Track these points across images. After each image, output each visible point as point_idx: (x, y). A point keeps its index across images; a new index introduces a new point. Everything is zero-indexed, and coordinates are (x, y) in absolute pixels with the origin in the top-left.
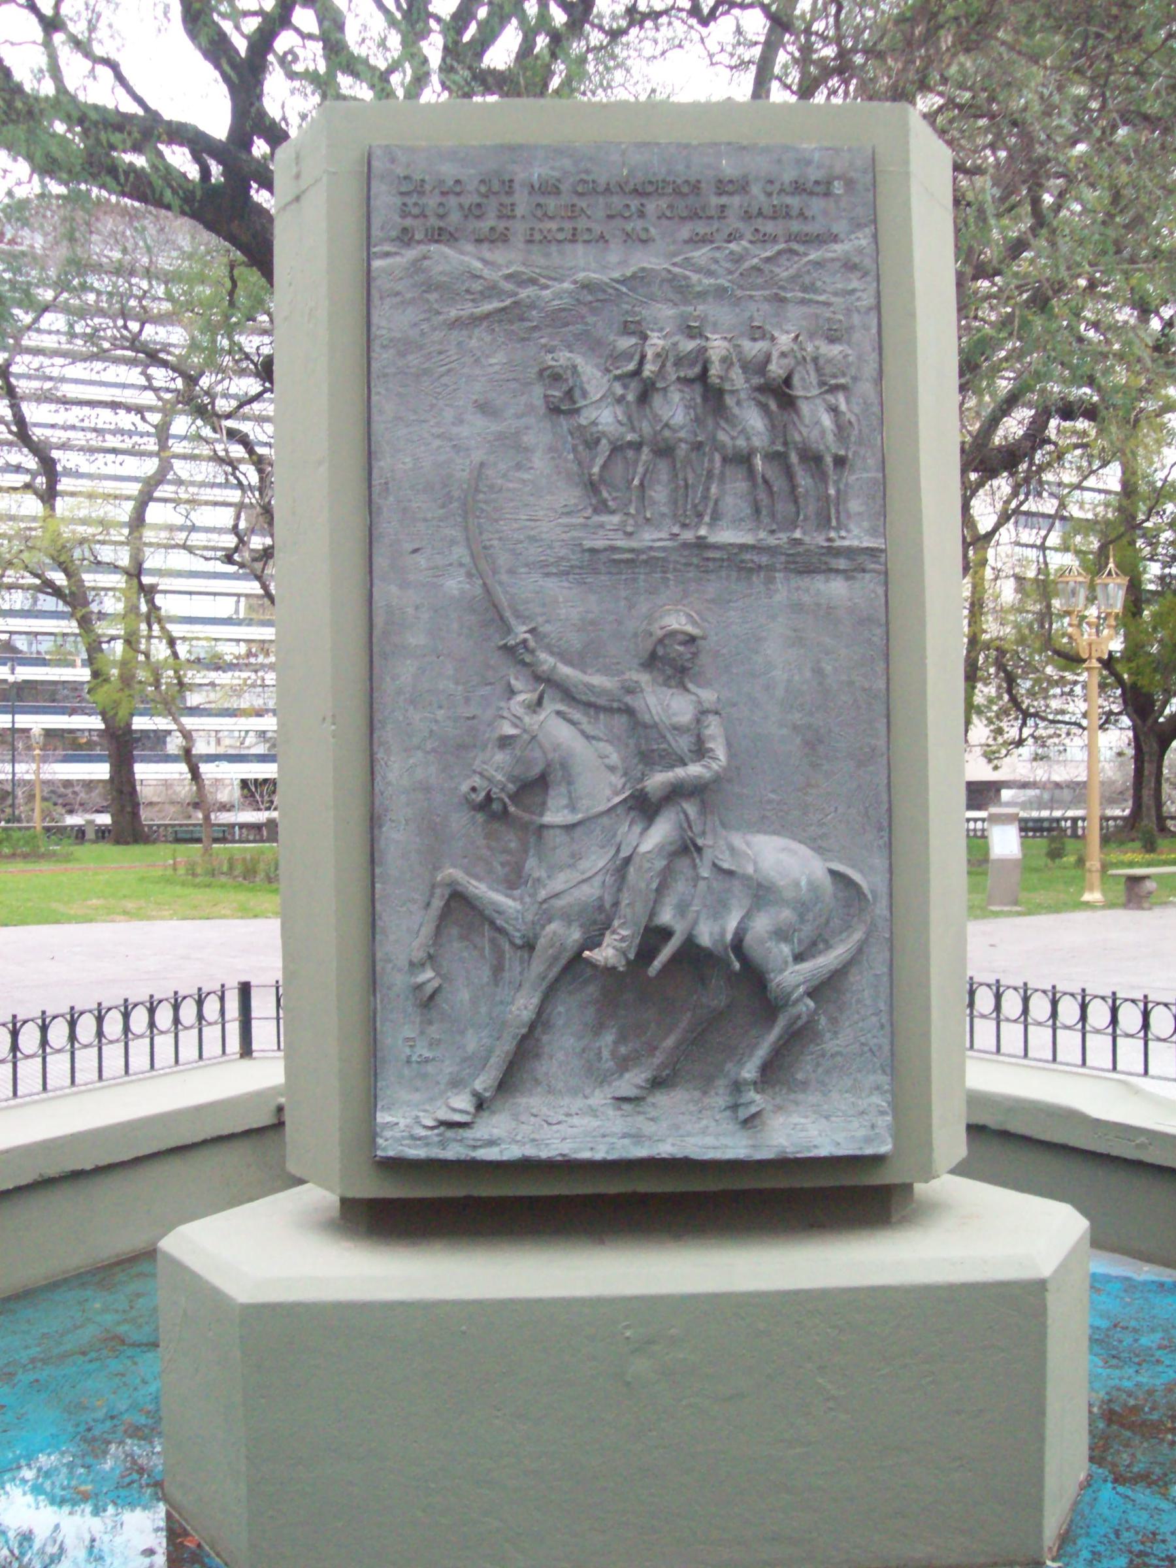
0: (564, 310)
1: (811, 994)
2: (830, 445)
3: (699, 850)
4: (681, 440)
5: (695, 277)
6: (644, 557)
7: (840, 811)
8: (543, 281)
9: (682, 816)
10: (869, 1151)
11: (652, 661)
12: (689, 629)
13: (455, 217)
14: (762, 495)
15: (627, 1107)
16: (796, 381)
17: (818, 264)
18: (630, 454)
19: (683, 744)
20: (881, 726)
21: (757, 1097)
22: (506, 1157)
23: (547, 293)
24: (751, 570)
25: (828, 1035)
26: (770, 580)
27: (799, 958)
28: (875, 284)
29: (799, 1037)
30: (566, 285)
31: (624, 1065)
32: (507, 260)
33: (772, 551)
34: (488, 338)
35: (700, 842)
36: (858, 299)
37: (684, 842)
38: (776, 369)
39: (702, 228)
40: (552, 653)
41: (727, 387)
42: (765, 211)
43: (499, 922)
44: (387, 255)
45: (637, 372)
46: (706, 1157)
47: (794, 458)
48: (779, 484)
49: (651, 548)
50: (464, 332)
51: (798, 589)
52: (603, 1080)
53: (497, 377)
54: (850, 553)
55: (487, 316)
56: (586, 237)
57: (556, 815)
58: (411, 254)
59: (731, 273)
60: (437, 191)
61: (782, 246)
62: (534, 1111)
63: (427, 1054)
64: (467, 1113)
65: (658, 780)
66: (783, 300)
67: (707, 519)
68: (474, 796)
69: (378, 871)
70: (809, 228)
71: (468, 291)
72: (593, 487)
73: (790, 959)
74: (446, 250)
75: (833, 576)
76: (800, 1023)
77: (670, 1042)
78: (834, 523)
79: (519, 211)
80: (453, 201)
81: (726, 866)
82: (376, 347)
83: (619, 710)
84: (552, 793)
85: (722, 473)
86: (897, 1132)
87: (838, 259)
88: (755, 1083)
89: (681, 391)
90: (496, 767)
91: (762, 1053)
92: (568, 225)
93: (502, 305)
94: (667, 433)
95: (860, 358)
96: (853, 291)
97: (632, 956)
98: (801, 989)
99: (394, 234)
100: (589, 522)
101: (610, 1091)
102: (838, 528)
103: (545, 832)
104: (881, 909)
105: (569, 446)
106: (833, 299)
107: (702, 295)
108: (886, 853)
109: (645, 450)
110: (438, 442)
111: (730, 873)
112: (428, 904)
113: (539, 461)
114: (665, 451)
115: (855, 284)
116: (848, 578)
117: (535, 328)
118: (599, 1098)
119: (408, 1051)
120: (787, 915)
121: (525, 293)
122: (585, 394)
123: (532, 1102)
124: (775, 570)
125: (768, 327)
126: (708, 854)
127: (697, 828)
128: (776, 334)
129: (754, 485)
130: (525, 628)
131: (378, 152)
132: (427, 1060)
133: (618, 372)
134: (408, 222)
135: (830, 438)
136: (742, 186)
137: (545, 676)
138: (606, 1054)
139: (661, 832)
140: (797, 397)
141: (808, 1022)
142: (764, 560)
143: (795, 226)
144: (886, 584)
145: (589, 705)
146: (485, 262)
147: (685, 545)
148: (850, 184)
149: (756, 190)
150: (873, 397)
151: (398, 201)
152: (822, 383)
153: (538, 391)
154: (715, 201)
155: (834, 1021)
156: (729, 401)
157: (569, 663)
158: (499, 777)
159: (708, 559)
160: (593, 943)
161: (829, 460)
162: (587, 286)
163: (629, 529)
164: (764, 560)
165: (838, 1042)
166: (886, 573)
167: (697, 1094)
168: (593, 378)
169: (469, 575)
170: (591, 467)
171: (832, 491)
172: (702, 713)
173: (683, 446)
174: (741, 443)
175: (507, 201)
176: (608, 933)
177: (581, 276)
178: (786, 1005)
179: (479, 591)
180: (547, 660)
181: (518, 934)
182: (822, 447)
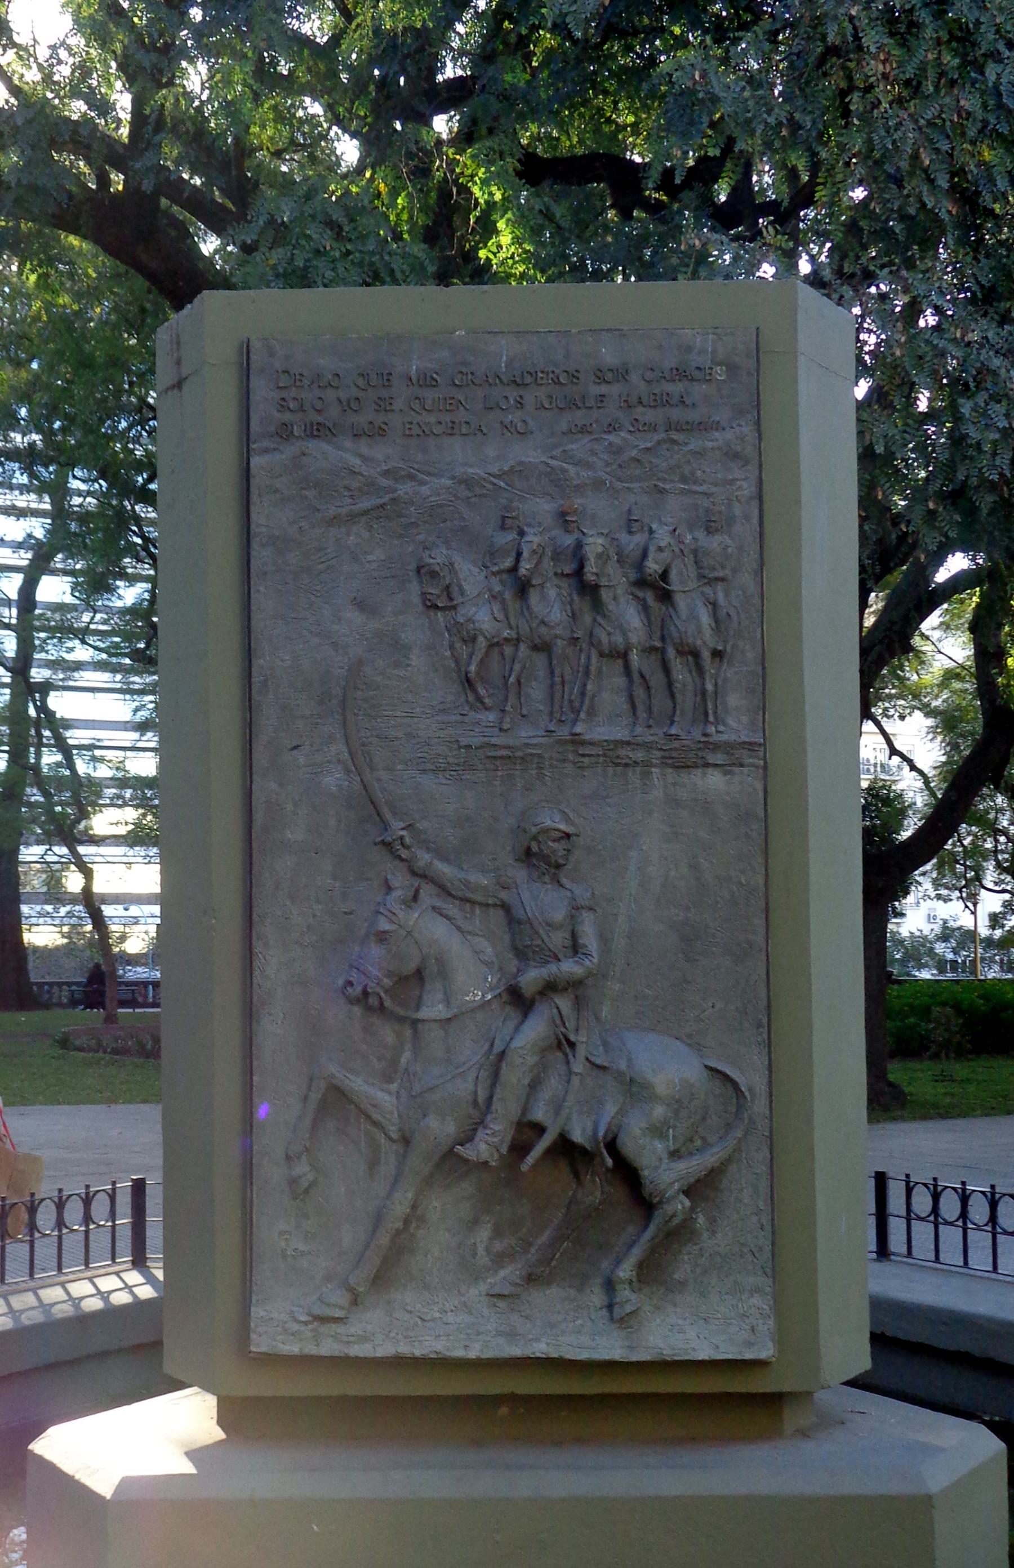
0: (441, 506)
1: (687, 1193)
2: (706, 638)
3: (572, 1045)
4: (556, 637)
5: (572, 470)
6: (519, 754)
7: (718, 1006)
8: (421, 476)
9: (555, 1011)
10: (748, 1356)
11: (528, 856)
12: (562, 827)
13: (334, 412)
14: (639, 692)
15: (502, 1304)
16: (673, 575)
17: (699, 454)
18: (508, 650)
19: (558, 939)
20: (759, 922)
21: (633, 1297)
22: (380, 1353)
23: (424, 490)
24: (626, 765)
25: (705, 1235)
26: (646, 775)
27: (675, 1155)
28: (757, 472)
29: (678, 1235)
30: (446, 482)
31: (499, 1260)
32: (384, 453)
33: (648, 747)
34: (366, 535)
35: (572, 1038)
36: (740, 488)
37: (558, 1038)
38: (653, 566)
39: (580, 417)
40: (429, 850)
41: (603, 582)
42: (645, 401)
43: (376, 1116)
44: (266, 451)
45: (514, 569)
46: (579, 1358)
47: (671, 653)
48: (657, 679)
49: (527, 745)
50: (343, 530)
51: (675, 784)
52: (476, 1276)
53: (375, 574)
54: (727, 748)
55: (365, 512)
56: (464, 431)
57: (433, 1009)
58: (290, 450)
59: (608, 464)
60: (315, 385)
61: (663, 435)
62: (409, 1308)
63: (301, 1247)
64: (342, 1308)
65: (532, 978)
66: (662, 491)
67: (582, 715)
68: (350, 989)
69: (255, 1063)
70: (693, 416)
71: (346, 488)
72: (468, 682)
73: (665, 1156)
74: (324, 446)
75: (710, 770)
76: (676, 1221)
77: (545, 1237)
78: (711, 718)
79: (399, 404)
80: (330, 394)
81: (598, 1062)
82: (255, 545)
83: (495, 905)
84: (428, 986)
85: (600, 671)
86: (780, 1338)
87: (719, 448)
88: (631, 1282)
89: (558, 587)
90: (376, 964)
91: (637, 1253)
92: (447, 418)
93: (380, 501)
94: (543, 630)
95: (740, 548)
96: (735, 480)
97: (504, 1150)
98: (676, 1186)
99: (272, 429)
100: (466, 719)
101: (483, 1287)
102: (717, 721)
103: (420, 1026)
104: (760, 1106)
105: (446, 643)
106: (714, 489)
107: (579, 489)
108: (765, 1051)
109: (522, 647)
110: (316, 640)
111: (602, 1068)
112: (306, 1098)
113: (417, 660)
114: (542, 647)
115: (737, 474)
116: (726, 773)
117: (415, 525)
118: (474, 1293)
119: (283, 1244)
120: (659, 1111)
121: (405, 489)
122: (462, 593)
123: (408, 1297)
124: (652, 765)
125: (646, 520)
126: (581, 1051)
127: (571, 1024)
128: (654, 526)
129: (631, 681)
130: (402, 825)
131: (256, 345)
132: (302, 1254)
133: (495, 569)
134: (287, 417)
135: (707, 633)
136: (621, 373)
137: (420, 872)
138: (481, 1251)
139: (536, 1029)
140: (673, 591)
141: (685, 1220)
142: (639, 755)
143: (676, 414)
144: (765, 777)
145: (465, 900)
146: (364, 459)
147: (562, 742)
148: (732, 369)
149: (634, 377)
150: (752, 588)
151: (277, 395)
152: (701, 577)
153: (415, 588)
154: (595, 390)
155: (712, 1221)
156: (605, 595)
157: (446, 860)
158: (375, 972)
159: (583, 755)
160: (467, 1138)
161: (706, 654)
162: (467, 482)
163: (506, 726)
164: (639, 755)
165: (717, 1240)
166: (765, 768)
167: (572, 1292)
168: (471, 576)
169: (348, 771)
170: (469, 664)
171: (710, 687)
172: (576, 909)
173: (559, 642)
174: (618, 639)
175: (384, 393)
176: (480, 1129)
177: (459, 471)
178: (660, 1202)
179: (357, 786)
180: (423, 858)
181: (393, 1128)
182: (699, 642)
